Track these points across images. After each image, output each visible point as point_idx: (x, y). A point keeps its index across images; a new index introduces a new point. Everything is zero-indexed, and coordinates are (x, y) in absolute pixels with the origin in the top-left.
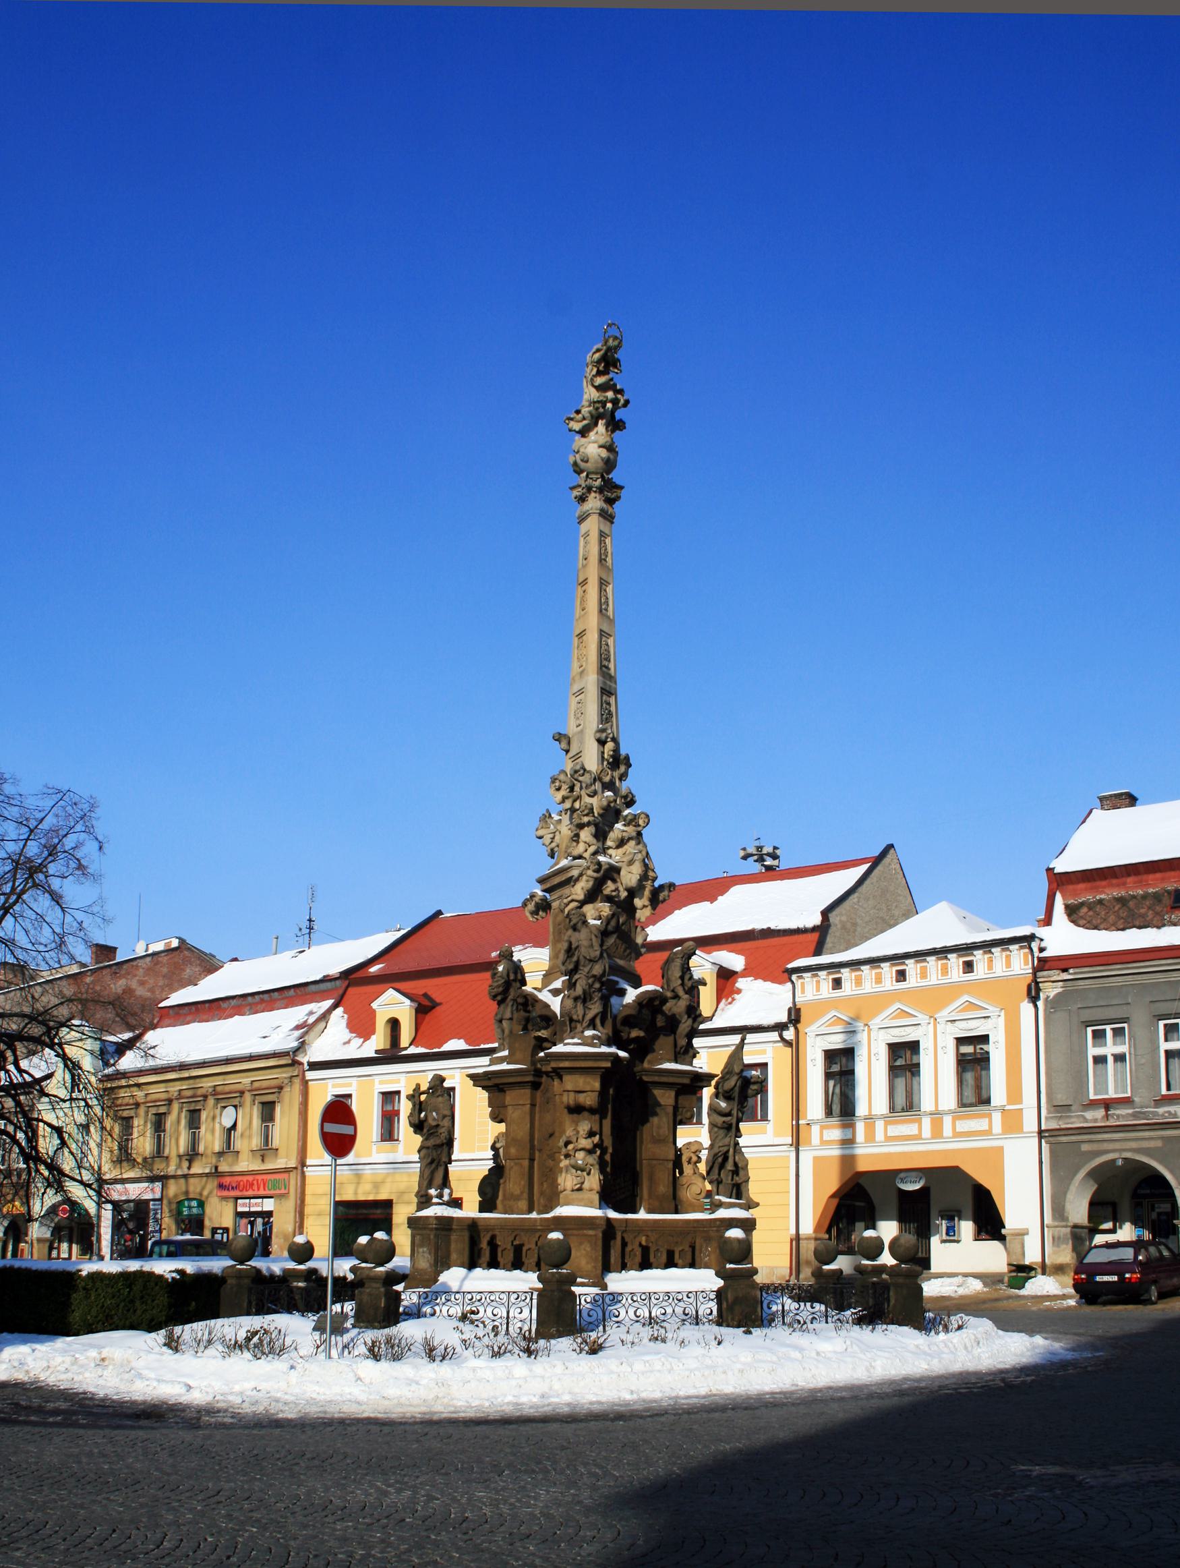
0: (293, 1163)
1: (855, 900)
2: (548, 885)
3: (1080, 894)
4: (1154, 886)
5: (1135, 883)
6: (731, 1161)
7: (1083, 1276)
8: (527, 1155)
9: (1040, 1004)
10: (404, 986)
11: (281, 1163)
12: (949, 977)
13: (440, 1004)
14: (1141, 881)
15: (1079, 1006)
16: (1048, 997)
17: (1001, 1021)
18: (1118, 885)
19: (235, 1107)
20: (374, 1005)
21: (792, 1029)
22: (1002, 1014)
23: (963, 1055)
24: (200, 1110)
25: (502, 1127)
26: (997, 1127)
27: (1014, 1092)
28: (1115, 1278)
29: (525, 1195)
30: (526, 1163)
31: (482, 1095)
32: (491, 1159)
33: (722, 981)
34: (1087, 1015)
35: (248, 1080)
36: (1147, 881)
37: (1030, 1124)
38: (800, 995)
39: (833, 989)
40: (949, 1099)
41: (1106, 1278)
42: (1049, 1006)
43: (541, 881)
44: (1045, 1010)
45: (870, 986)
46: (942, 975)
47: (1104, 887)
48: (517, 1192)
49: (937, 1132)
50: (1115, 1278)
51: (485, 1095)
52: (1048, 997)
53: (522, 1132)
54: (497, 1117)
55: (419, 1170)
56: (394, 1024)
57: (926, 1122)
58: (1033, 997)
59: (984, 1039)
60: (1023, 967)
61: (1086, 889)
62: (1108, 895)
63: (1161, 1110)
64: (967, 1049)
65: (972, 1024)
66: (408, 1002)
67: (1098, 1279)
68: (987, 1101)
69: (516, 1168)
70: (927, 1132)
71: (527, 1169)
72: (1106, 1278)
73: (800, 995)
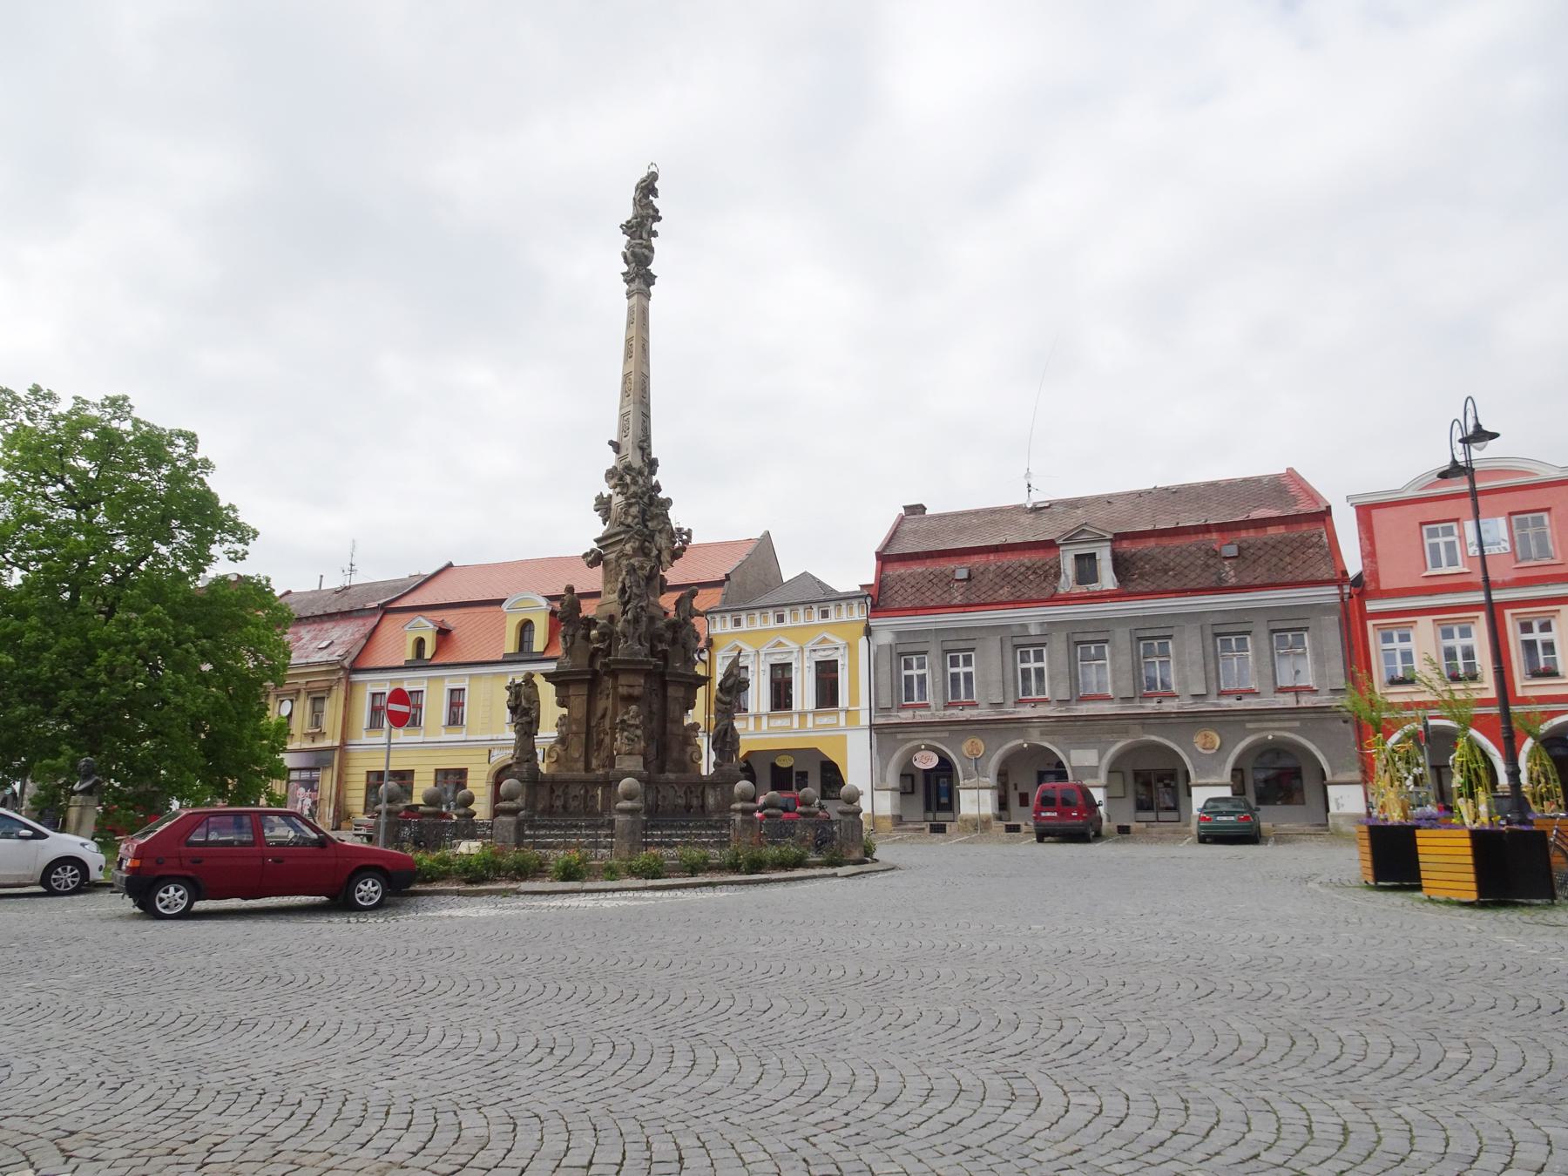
0: (337, 743)
2: (604, 544)
6: (729, 735)
8: (584, 730)
11: (326, 743)
19: (292, 701)
21: (707, 653)
24: (323, 698)
25: (565, 711)
26: (842, 723)
27: (854, 698)
28: (1043, 814)
29: (582, 759)
30: (583, 736)
31: (551, 688)
34: (950, 646)
35: (304, 681)
37: (864, 720)
40: (810, 703)
41: (1048, 814)
43: (597, 541)
48: (577, 755)
49: (802, 723)
50: (1043, 814)
51: (554, 687)
53: (580, 713)
54: (561, 704)
57: (796, 718)
63: (948, 712)
65: (778, 657)
67: (1055, 814)
68: (789, 706)
69: (575, 739)
70: (796, 725)
71: (584, 741)
72: (1048, 814)
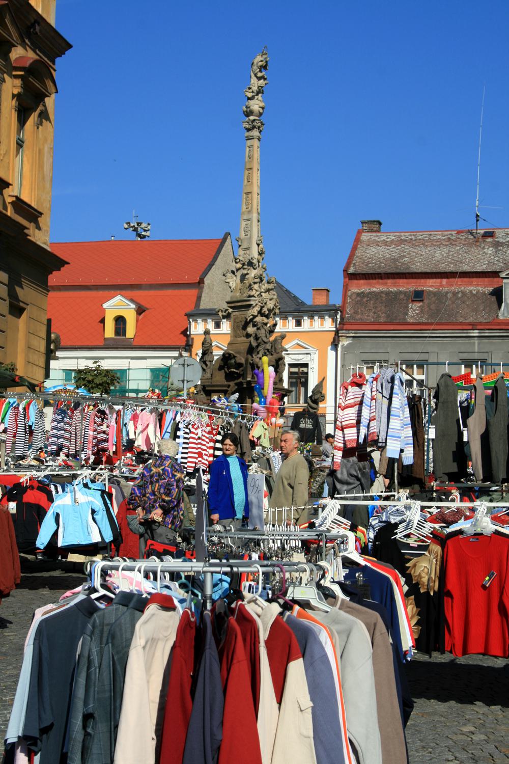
1: (214, 270)
3: (361, 286)
4: (403, 287)
5: (392, 283)
7: (224, 473)
9: (339, 349)
10: (129, 293)
12: (324, 327)
13: (148, 309)
14: (395, 283)
15: (451, 351)
16: (343, 345)
17: (316, 357)
18: (382, 284)
20: (105, 306)
22: (317, 352)
23: (291, 372)
32: (393, 415)
33: (138, 316)
36: (399, 283)
38: (194, 330)
39: (296, 326)
42: (344, 350)
44: (342, 352)
45: (292, 328)
46: (283, 326)
47: (375, 284)
52: (343, 345)
55: (409, 419)
56: (120, 321)
58: (335, 345)
59: (306, 365)
60: (330, 326)
61: (364, 284)
62: (377, 289)
64: (295, 370)
65: (300, 357)
66: (133, 306)
73: (194, 330)
